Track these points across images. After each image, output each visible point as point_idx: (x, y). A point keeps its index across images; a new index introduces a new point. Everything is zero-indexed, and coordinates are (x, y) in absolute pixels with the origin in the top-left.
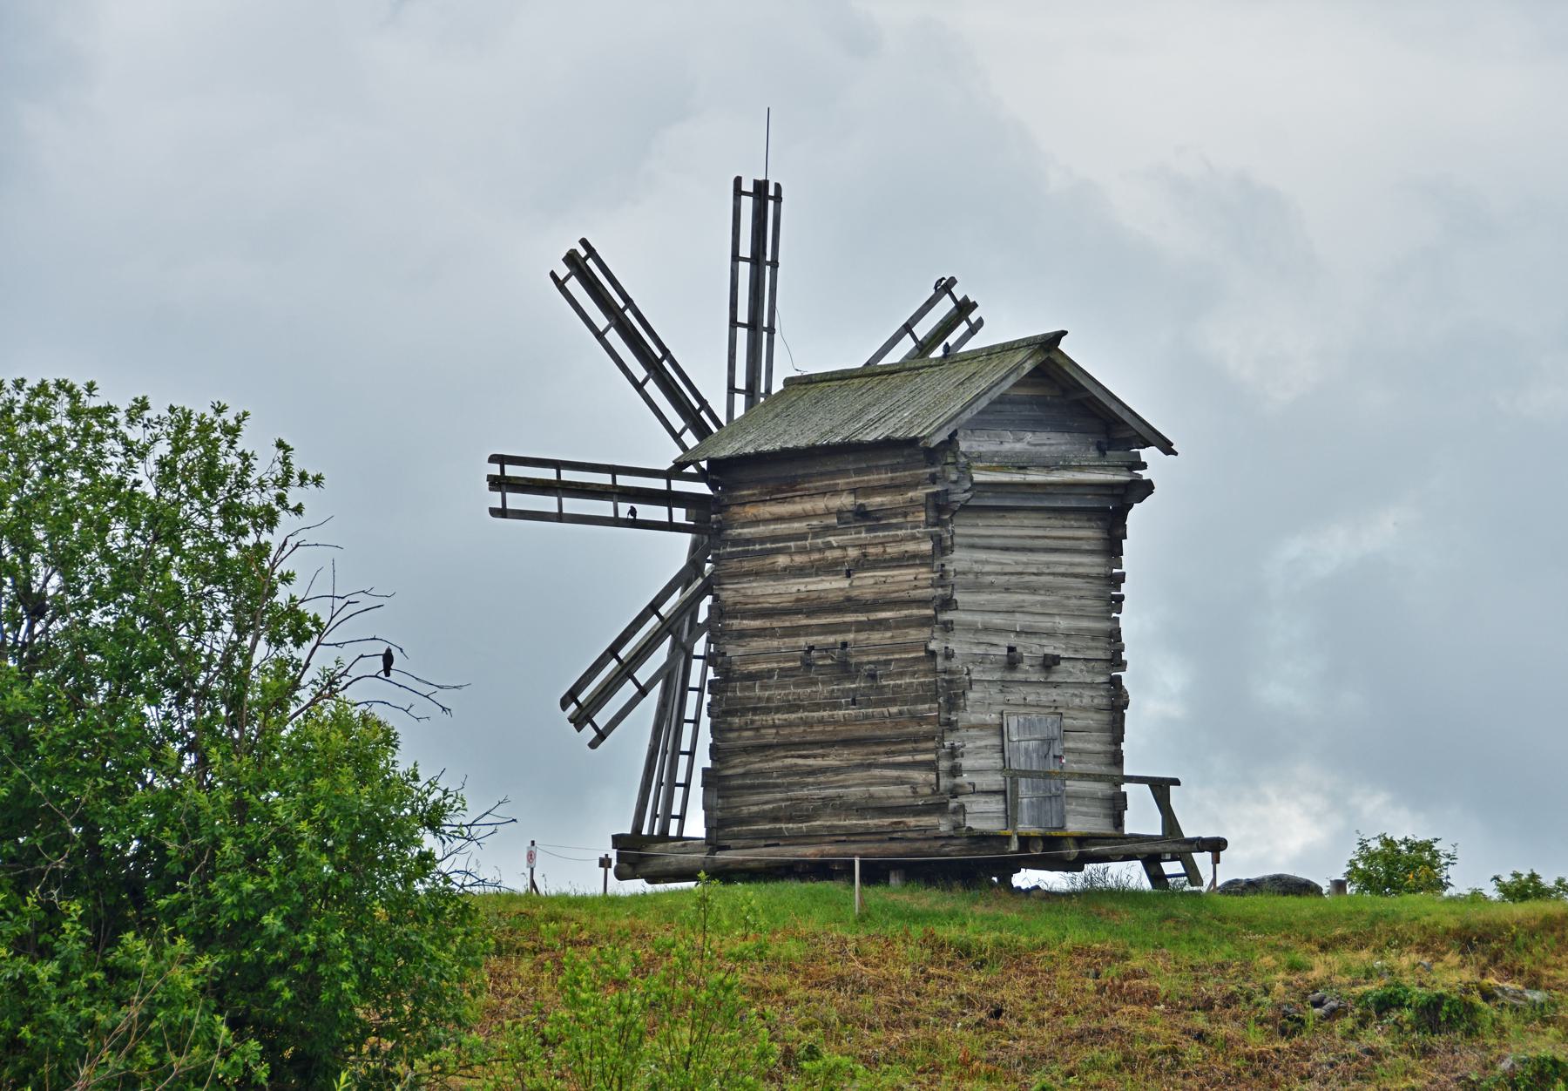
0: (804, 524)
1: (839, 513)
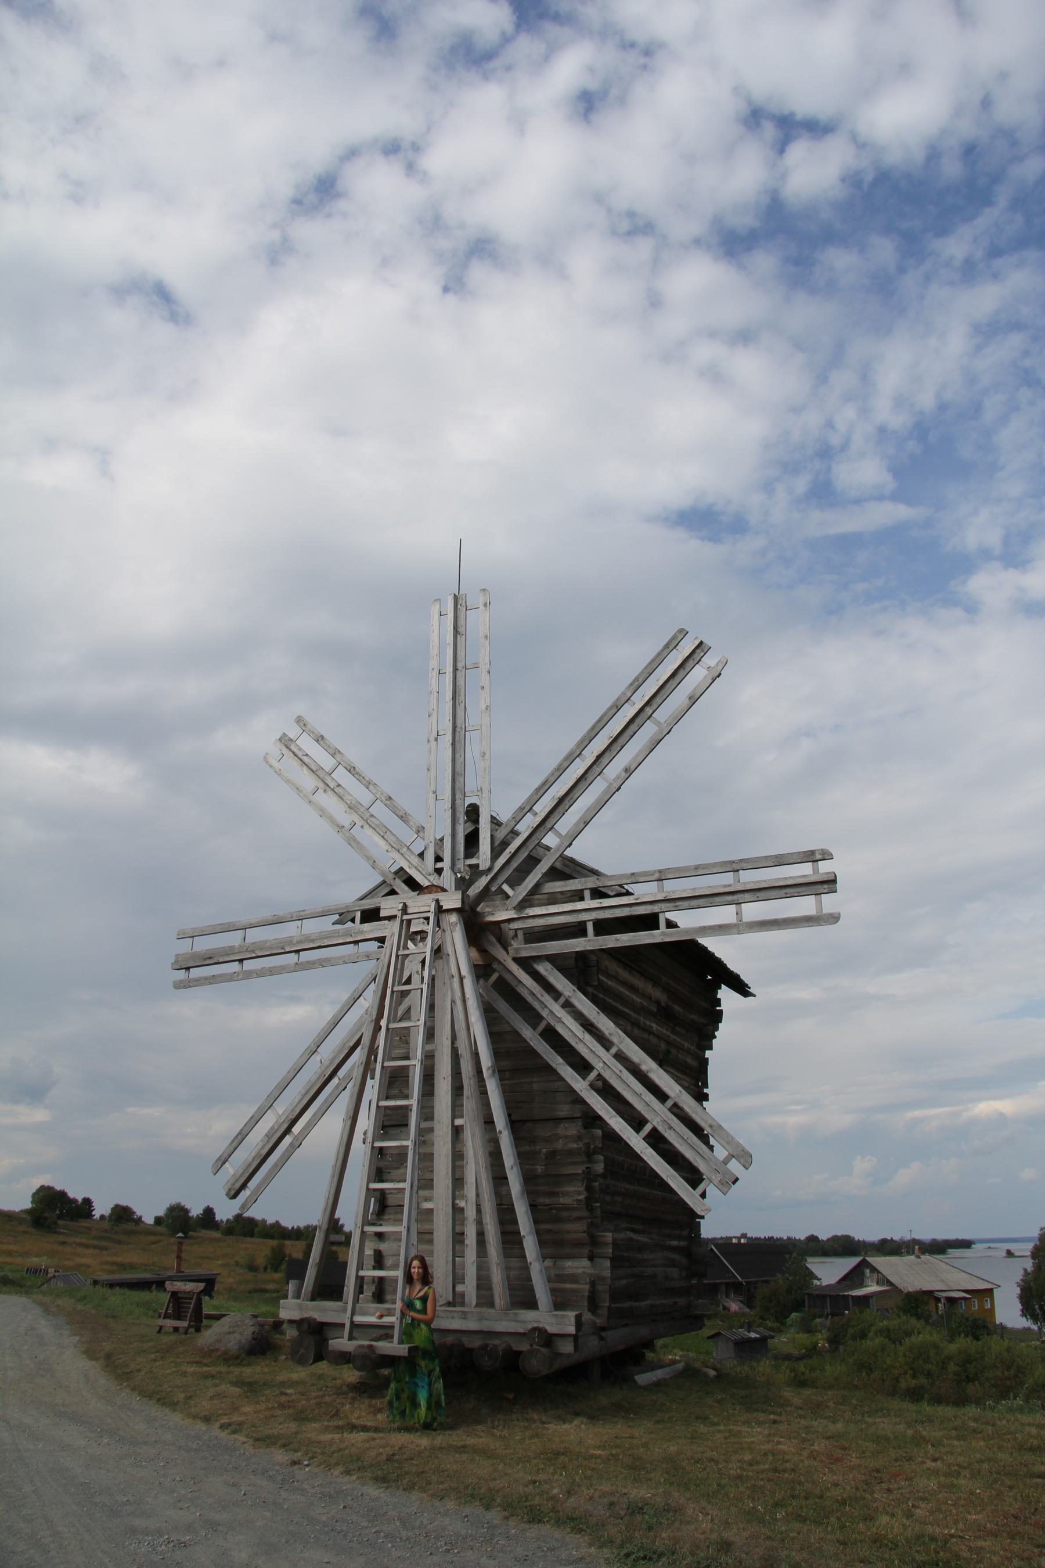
0: (639, 1000)
1: (658, 1003)
